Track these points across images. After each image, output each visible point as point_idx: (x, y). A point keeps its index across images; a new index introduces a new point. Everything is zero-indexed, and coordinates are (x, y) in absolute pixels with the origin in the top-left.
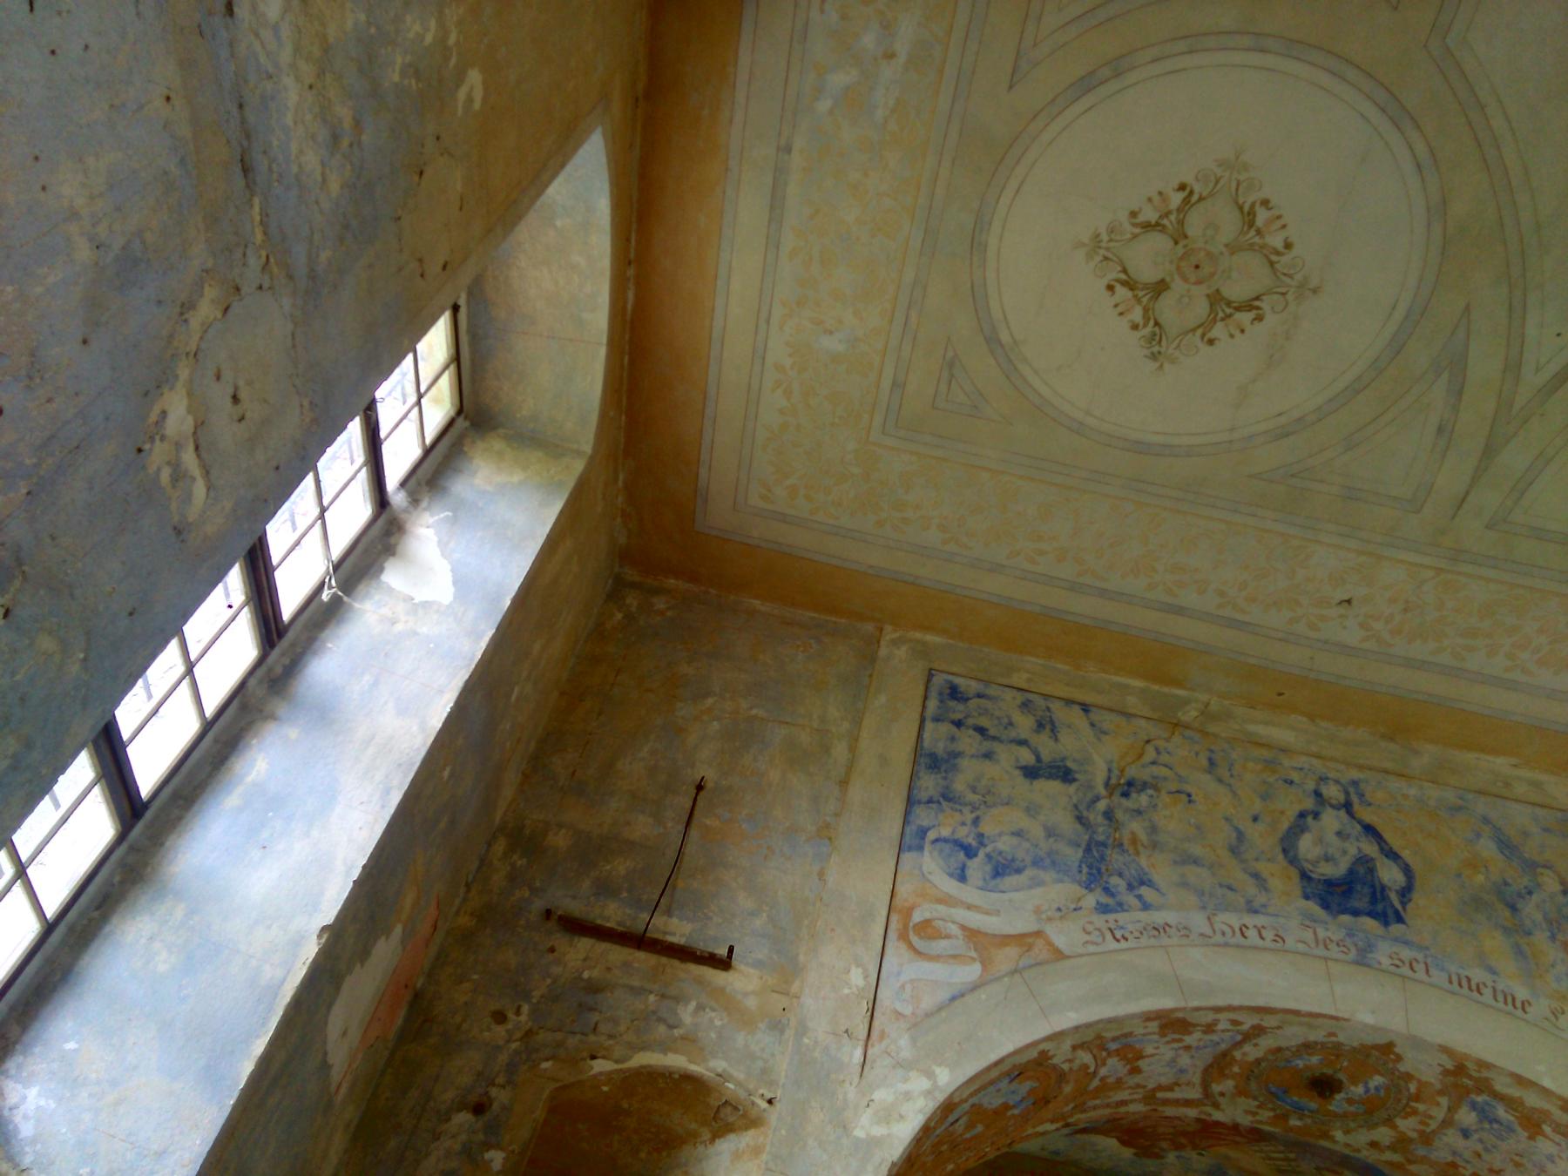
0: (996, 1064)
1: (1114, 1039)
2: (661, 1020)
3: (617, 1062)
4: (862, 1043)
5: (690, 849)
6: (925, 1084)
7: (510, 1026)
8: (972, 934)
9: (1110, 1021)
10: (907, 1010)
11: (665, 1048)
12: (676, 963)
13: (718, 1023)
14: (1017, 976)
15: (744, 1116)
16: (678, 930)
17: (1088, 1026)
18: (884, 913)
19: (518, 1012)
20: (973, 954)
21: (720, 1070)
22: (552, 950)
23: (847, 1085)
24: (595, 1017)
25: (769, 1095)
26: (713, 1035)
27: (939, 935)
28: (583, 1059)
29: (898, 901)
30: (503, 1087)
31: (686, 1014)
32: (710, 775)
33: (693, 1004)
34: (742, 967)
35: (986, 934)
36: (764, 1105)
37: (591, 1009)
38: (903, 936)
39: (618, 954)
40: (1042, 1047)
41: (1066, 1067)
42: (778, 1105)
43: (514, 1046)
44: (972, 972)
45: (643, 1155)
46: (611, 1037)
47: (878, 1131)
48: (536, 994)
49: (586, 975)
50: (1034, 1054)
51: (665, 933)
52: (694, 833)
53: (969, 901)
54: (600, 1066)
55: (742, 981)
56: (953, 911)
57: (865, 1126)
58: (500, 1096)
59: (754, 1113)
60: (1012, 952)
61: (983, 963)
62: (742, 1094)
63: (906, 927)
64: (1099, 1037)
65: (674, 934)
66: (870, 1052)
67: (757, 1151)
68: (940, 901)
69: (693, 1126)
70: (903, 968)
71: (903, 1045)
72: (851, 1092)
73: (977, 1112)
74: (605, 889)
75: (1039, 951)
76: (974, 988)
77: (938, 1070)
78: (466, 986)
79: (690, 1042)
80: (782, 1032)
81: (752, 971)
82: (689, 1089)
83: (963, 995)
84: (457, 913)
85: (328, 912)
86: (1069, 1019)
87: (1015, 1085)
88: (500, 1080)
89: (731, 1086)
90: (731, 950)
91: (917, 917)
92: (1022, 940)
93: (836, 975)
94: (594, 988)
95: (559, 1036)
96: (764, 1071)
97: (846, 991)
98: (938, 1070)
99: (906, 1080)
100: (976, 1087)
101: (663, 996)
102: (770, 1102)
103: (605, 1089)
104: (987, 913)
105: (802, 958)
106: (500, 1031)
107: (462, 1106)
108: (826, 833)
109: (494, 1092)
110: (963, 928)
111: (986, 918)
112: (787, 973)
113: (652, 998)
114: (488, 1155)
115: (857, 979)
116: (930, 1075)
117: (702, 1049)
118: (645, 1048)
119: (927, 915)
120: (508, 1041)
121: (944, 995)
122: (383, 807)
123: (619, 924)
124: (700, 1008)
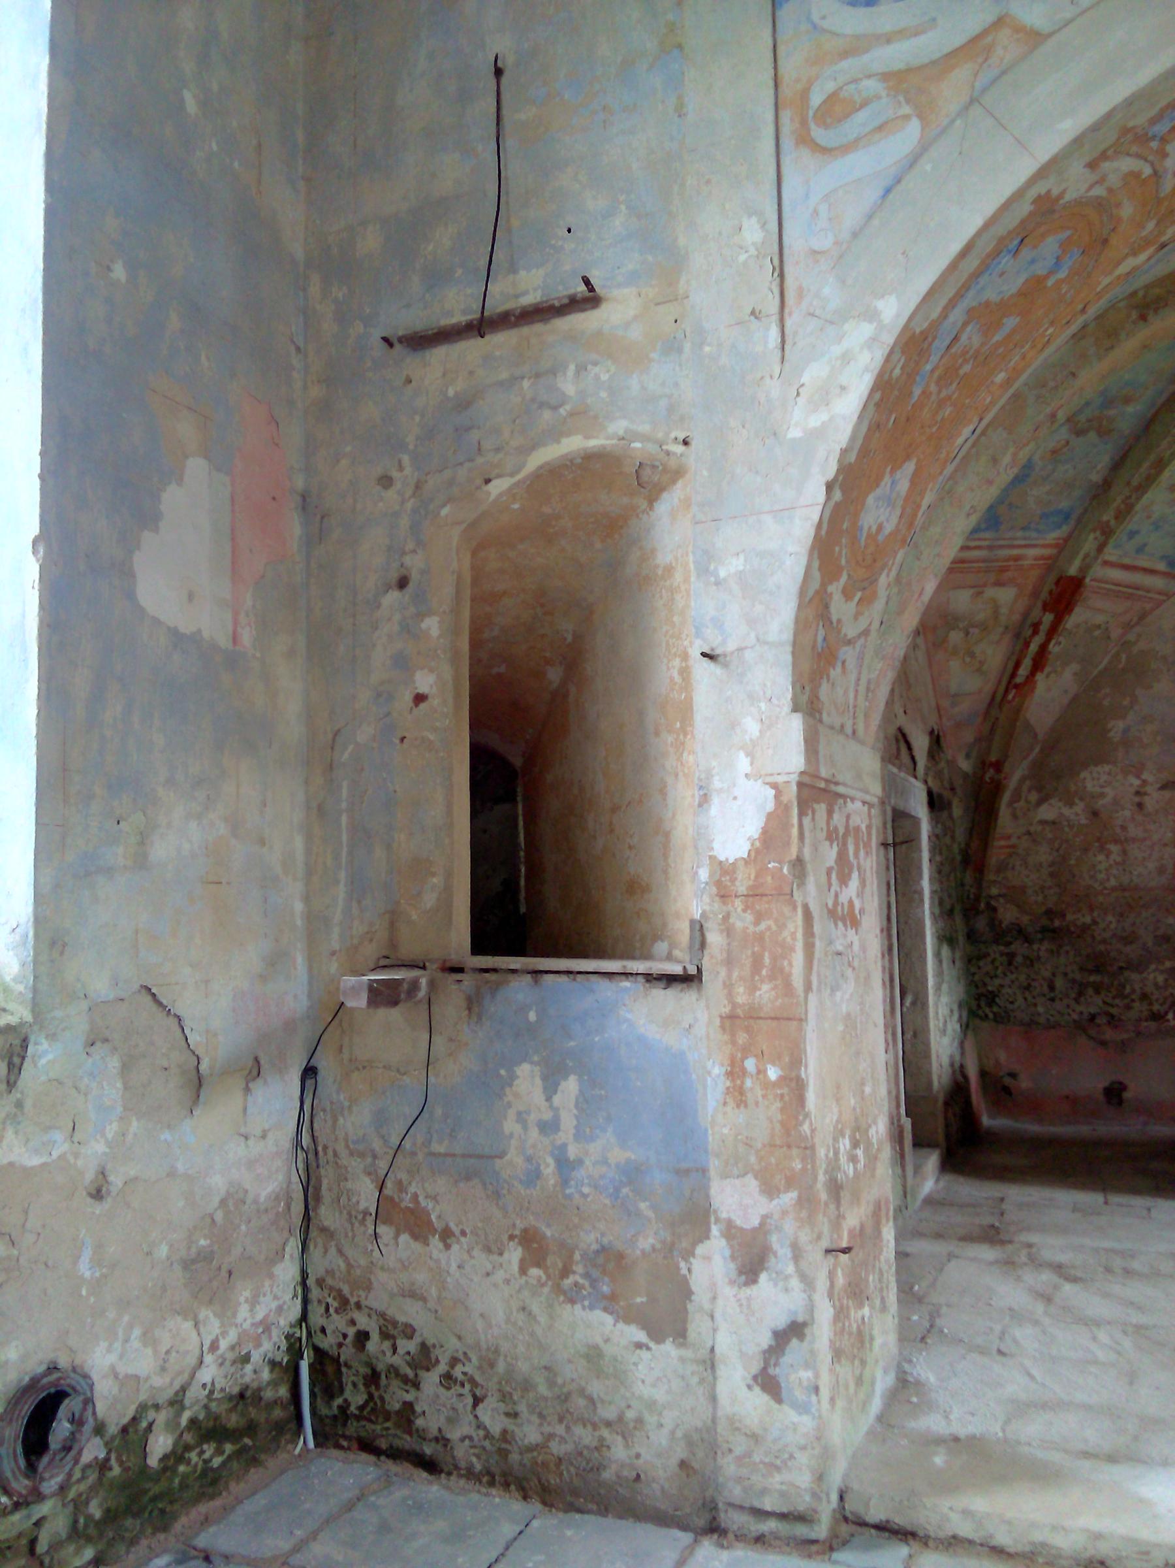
0: (953, 266)
1: (1153, 121)
2: (542, 405)
3: (512, 475)
4: (775, 318)
5: (512, 168)
6: (867, 330)
7: (398, 485)
8: (898, 80)
9: (1129, 102)
10: (825, 242)
11: (556, 434)
12: (538, 327)
13: (604, 377)
14: (976, 110)
15: (665, 470)
16: (528, 285)
17: (1095, 128)
18: (770, 116)
19: (401, 468)
20: (906, 110)
21: (621, 433)
22: (409, 381)
23: (768, 380)
24: (475, 435)
25: (681, 436)
26: (603, 394)
27: (854, 107)
28: (478, 488)
29: (786, 91)
30: (414, 551)
31: (568, 385)
32: (503, 44)
33: (572, 367)
34: (615, 293)
35: (919, 68)
36: (680, 449)
37: (468, 429)
38: (804, 140)
39: (471, 349)
40: (1041, 188)
41: (1099, 191)
42: (694, 443)
43: (409, 505)
44: (910, 134)
45: (598, 546)
46: (498, 450)
47: (815, 421)
48: (410, 439)
49: (451, 392)
50: (1025, 208)
51: (517, 296)
52: (509, 143)
53: (888, 28)
54: (498, 487)
55: (619, 312)
56: (866, 58)
57: (800, 421)
58: (414, 563)
59: (673, 463)
60: (962, 74)
61: (921, 117)
62: (652, 448)
63: (804, 123)
64: (1125, 131)
65: (526, 293)
66: (789, 323)
67: (687, 503)
68: (845, 54)
69: (625, 500)
70: (810, 182)
71: (830, 293)
72: (774, 389)
73: (988, 315)
74: (436, 277)
75: (1006, 47)
76: (914, 160)
77: (880, 304)
78: (344, 462)
79: (584, 416)
80: (680, 351)
81: (626, 291)
82: (596, 467)
83: (899, 181)
84: (305, 387)
85: (32, 525)
86: (1068, 128)
87: (1026, 253)
88: (410, 546)
89: (638, 445)
90: (587, 282)
91: (816, 99)
92: (976, 47)
93: (725, 237)
94: (464, 403)
95: (447, 474)
96: (671, 409)
97: (743, 257)
98: (880, 304)
99: (840, 339)
100: (950, 292)
101: (538, 375)
102: (685, 443)
103: (516, 506)
104: (916, 34)
105: (682, 241)
106: (391, 494)
107: (388, 588)
108: (672, 44)
109: (408, 560)
110: (886, 77)
111: (922, 40)
112: (667, 270)
113: (526, 384)
114: (424, 625)
115: (753, 233)
116: (871, 315)
117: (596, 417)
118: (534, 447)
119: (830, 87)
120: (403, 502)
121: (872, 195)
122: (29, 372)
123: (464, 312)
124: (581, 369)
